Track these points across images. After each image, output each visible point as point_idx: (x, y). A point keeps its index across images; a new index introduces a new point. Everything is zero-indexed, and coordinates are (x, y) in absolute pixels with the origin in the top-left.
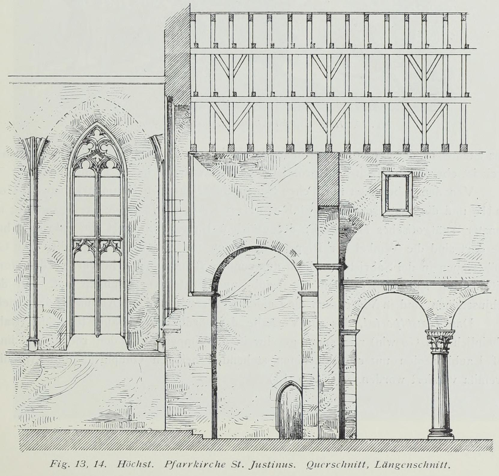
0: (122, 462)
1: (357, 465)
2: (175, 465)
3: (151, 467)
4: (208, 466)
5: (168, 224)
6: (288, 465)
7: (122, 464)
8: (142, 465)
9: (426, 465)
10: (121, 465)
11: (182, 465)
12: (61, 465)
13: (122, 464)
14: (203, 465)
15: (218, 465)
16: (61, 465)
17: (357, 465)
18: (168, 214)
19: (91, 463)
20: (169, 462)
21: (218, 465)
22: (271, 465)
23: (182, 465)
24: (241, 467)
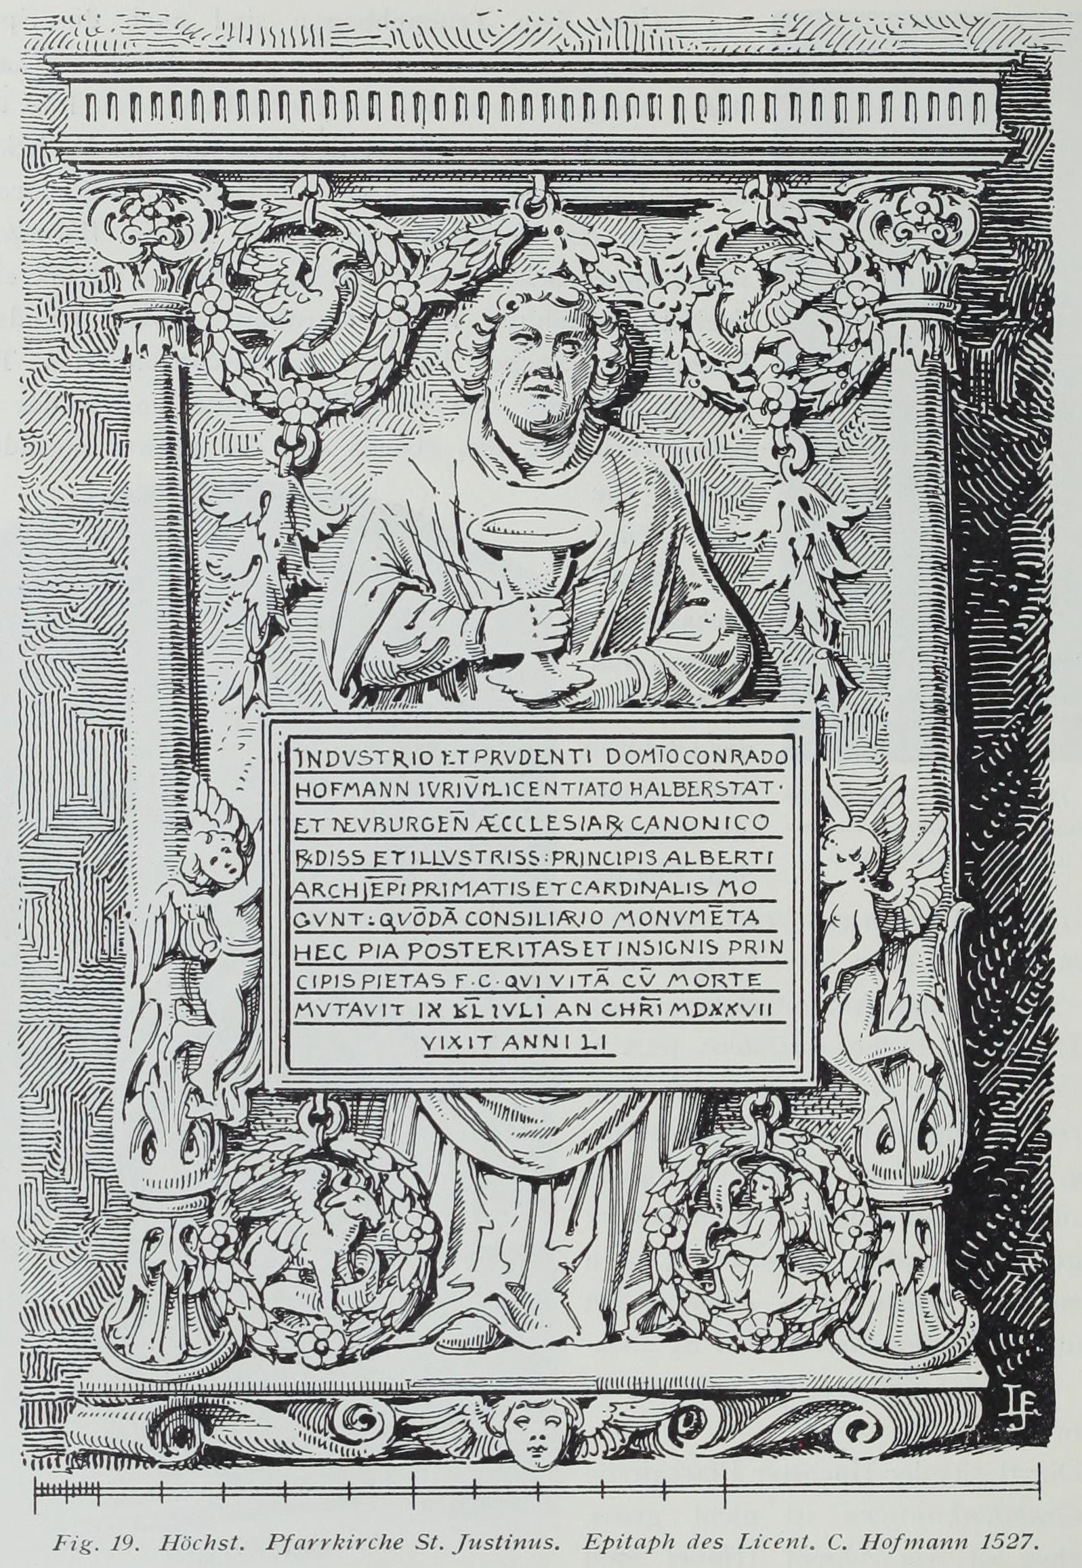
0: (172, 1539)
1: (623, 1544)
2: (292, 1544)
3: (807, 1548)
4: (365, 1545)
5: (111, 163)
6: (543, 1544)
7: (170, 1543)
8: (217, 1545)
9: (664, 1489)
10: (172, 1539)
11: (307, 1545)
12: (78, 1546)
13: (170, 1543)
14: (354, 1544)
15: (386, 1543)
16: (78, 1546)
17: (623, 1544)
18: (999, 470)
19: (149, 1541)
20: (278, 1538)
21: (386, 1543)
22: (503, 1543)
23: (307, 1545)
24: (437, 1548)
